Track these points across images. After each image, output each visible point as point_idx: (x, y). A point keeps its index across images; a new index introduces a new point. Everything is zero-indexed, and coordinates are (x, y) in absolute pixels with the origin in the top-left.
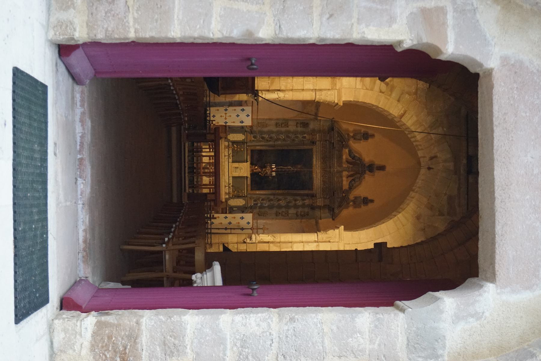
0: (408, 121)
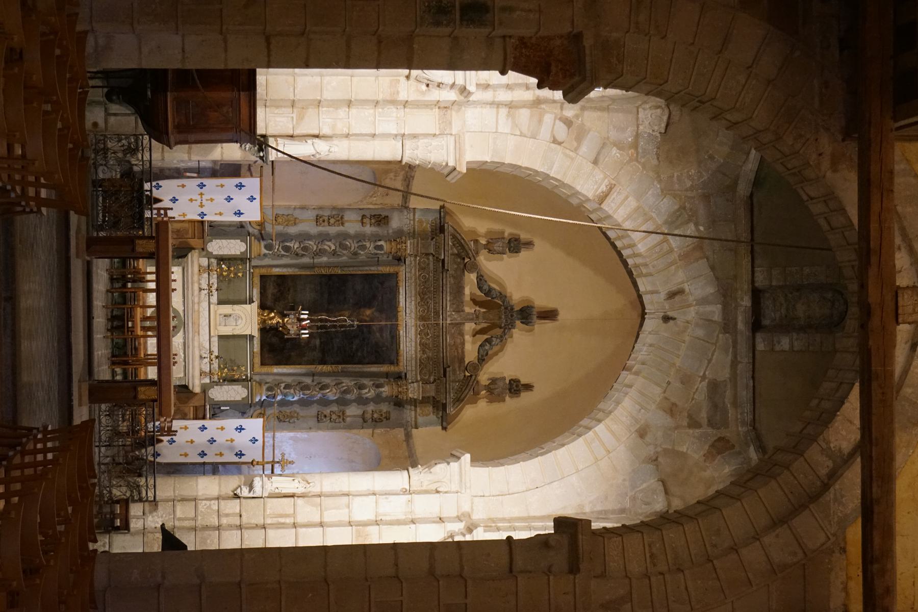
0: (618, 207)
